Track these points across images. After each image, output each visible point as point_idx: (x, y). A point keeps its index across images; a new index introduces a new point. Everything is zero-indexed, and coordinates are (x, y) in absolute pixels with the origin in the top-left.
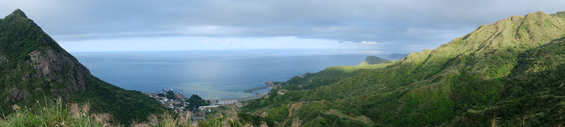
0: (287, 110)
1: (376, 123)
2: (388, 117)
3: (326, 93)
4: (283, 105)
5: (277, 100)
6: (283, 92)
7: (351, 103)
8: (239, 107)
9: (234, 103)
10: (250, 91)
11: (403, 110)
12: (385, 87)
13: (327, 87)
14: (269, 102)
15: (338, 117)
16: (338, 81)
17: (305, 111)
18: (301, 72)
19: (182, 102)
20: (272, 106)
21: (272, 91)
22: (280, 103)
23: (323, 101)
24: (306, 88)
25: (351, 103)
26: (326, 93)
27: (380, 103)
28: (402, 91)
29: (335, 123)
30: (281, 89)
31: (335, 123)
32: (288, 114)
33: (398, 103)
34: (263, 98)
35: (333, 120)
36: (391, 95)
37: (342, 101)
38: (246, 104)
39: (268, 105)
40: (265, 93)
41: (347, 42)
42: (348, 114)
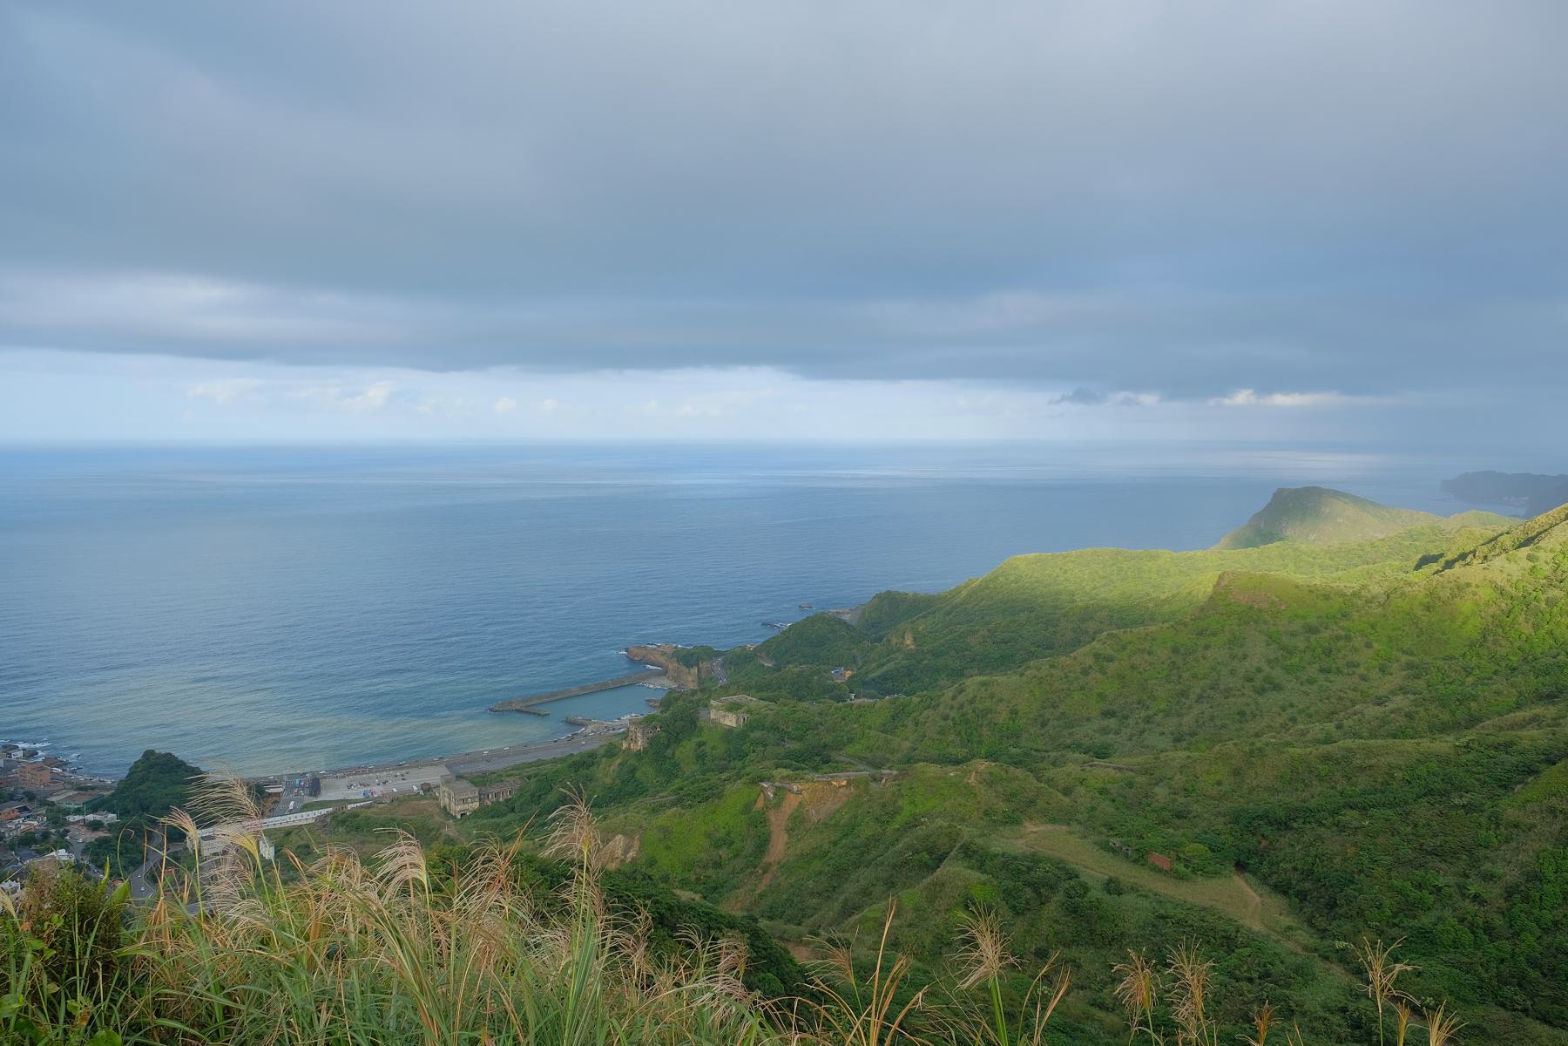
0: (758, 824)
1: (1323, 933)
2: (1410, 908)
3: (1002, 717)
4: (736, 794)
5: (701, 757)
6: (734, 708)
7: (1161, 792)
8: (456, 809)
9: (427, 788)
10: (527, 708)
11: (1536, 877)
12: (1399, 701)
13: (1005, 681)
14: (646, 773)
15: (1072, 875)
16: (1077, 643)
17: (868, 830)
18: (857, 577)
19: (58, 817)
20: (666, 796)
21: (666, 704)
22: (714, 778)
23: (983, 765)
24: (883, 685)
25: (1161, 792)
26: (1002, 717)
27: (1364, 809)
28: (1533, 738)
29: (1052, 910)
30: (725, 689)
31: (1052, 910)
32: (763, 845)
33: (1496, 820)
34: (611, 752)
35: (1041, 889)
36: (1444, 760)
37: (1103, 772)
38: (503, 792)
39: (640, 790)
40: (621, 719)
41: (1121, 395)
42: (1140, 858)
